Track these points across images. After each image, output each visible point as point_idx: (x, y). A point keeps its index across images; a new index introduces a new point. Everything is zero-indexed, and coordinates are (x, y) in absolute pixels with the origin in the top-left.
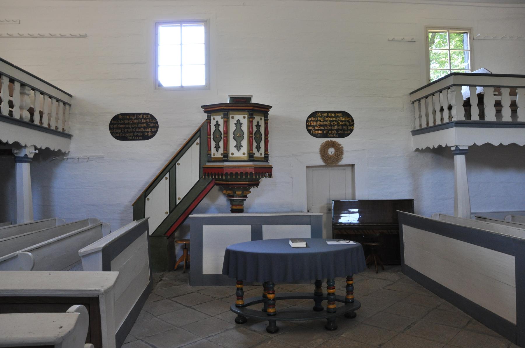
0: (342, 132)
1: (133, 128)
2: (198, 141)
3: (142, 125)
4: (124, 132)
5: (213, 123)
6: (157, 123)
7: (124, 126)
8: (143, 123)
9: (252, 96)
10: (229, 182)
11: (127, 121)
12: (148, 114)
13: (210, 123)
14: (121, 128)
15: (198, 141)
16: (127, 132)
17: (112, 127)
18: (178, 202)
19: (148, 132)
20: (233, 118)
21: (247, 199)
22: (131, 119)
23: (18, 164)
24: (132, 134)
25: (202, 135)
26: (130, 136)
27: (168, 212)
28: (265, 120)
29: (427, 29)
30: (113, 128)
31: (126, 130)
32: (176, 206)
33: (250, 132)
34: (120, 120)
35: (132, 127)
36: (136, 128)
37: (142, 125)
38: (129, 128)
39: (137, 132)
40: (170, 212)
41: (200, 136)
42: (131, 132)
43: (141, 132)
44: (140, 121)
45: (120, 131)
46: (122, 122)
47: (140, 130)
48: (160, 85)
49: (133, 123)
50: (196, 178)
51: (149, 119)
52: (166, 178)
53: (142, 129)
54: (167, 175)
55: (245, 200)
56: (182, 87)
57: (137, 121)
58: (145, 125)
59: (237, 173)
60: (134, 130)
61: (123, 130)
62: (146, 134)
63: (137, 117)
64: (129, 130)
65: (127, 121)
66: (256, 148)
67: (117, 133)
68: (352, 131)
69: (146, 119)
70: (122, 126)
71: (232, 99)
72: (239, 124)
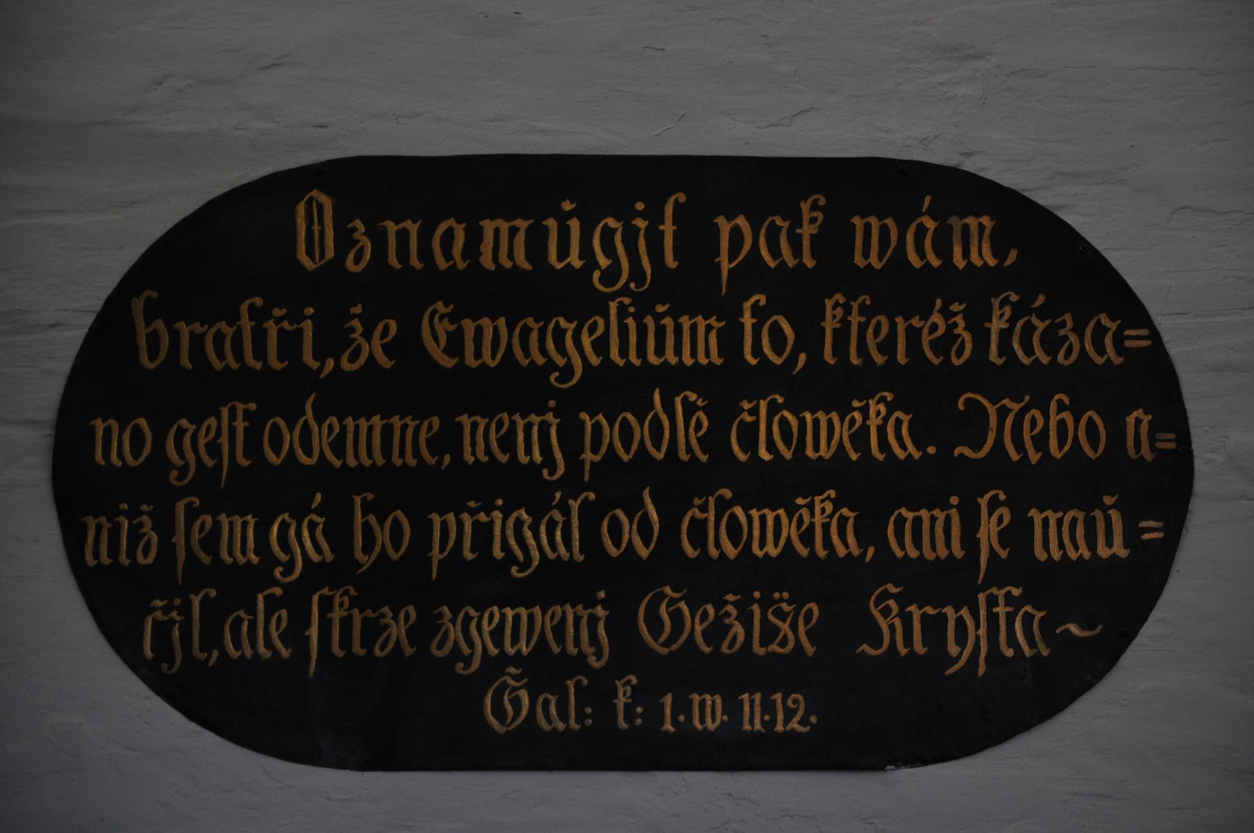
1: (618, 483)
3: (827, 435)
4: (383, 585)
7: (412, 438)
8: (833, 388)
11: (488, 340)
12: (957, 190)
14: (336, 487)
16: (482, 581)
17: (114, 445)
19: (951, 582)
22: (573, 296)
24: (583, 629)
30: (149, 485)
31: (453, 530)
34: (329, 292)
36: (678, 484)
37: (827, 435)
38: (521, 487)
39: (705, 581)
42: (553, 583)
43: (790, 575)
44: (764, 338)
46: (372, 349)
47: (771, 532)
49: (616, 388)
51: (975, 290)
57: (698, 341)
58: (888, 429)
60: (630, 537)
61: (379, 536)
62: (895, 627)
63: (697, 240)
64: (532, 540)
65: (488, 340)
67: (239, 586)
69: (902, 290)
70: (366, 439)
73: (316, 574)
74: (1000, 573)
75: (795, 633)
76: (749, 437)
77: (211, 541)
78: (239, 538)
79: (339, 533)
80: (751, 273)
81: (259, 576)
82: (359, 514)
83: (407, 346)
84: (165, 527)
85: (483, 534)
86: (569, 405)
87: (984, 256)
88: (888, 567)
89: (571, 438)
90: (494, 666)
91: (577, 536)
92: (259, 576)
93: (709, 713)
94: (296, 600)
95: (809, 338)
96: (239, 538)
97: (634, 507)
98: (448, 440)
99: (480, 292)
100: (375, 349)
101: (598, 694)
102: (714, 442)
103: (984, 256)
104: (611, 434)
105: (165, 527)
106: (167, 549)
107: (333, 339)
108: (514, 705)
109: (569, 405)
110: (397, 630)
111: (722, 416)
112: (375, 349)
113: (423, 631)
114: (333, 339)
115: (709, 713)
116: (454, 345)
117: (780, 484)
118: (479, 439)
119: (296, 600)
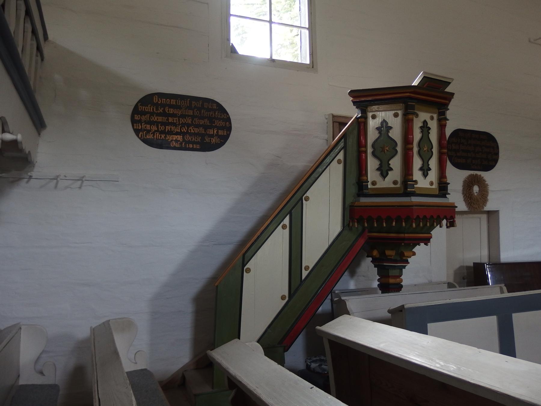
1: (183, 125)
3: (202, 122)
5: (373, 124)
7: (164, 119)
9: (453, 79)
10: (406, 235)
11: (171, 111)
13: (365, 124)
14: (157, 123)
15: (341, 156)
16: (171, 133)
18: (305, 274)
19: (212, 136)
20: (395, 182)
21: (408, 267)
24: (180, 138)
25: (350, 143)
26: (176, 141)
27: (287, 294)
28: (439, 120)
29: (313, 64)
34: (157, 105)
35: (185, 122)
36: (189, 126)
37: (202, 122)
39: (191, 134)
45: (154, 128)
46: (161, 111)
48: (233, 50)
50: (337, 228)
52: (284, 227)
53: (202, 131)
54: (286, 221)
55: (404, 267)
56: (273, 61)
57: (191, 113)
59: (432, 217)
61: (162, 128)
62: (207, 140)
65: (171, 111)
66: (421, 169)
67: (148, 131)
68: (496, 161)
70: (160, 119)
71: (426, 79)
72: (384, 170)
73: (155, 131)
74: (216, 135)
75: (199, 139)
76: (195, 121)
77: (146, 127)
78: (148, 127)
79: (158, 127)
82: (415, 200)
83: (164, 110)
84: (141, 125)
85: (171, 128)
86: (179, 117)
87: (215, 107)
89: (179, 120)
90: (172, 140)
91: (493, 296)
93: (191, 146)
94: (153, 133)
95: (200, 113)
97: (185, 127)
98: (168, 120)
99: (171, 106)
100: (161, 111)
101: (181, 144)
102: (192, 122)
103: (215, 107)
104: (183, 120)
105: (141, 125)
106: (142, 127)
107: (157, 109)
109: (179, 117)
110: (163, 136)
112: (161, 111)
114: (157, 109)
116: (168, 111)
117: (197, 126)
118: (171, 120)
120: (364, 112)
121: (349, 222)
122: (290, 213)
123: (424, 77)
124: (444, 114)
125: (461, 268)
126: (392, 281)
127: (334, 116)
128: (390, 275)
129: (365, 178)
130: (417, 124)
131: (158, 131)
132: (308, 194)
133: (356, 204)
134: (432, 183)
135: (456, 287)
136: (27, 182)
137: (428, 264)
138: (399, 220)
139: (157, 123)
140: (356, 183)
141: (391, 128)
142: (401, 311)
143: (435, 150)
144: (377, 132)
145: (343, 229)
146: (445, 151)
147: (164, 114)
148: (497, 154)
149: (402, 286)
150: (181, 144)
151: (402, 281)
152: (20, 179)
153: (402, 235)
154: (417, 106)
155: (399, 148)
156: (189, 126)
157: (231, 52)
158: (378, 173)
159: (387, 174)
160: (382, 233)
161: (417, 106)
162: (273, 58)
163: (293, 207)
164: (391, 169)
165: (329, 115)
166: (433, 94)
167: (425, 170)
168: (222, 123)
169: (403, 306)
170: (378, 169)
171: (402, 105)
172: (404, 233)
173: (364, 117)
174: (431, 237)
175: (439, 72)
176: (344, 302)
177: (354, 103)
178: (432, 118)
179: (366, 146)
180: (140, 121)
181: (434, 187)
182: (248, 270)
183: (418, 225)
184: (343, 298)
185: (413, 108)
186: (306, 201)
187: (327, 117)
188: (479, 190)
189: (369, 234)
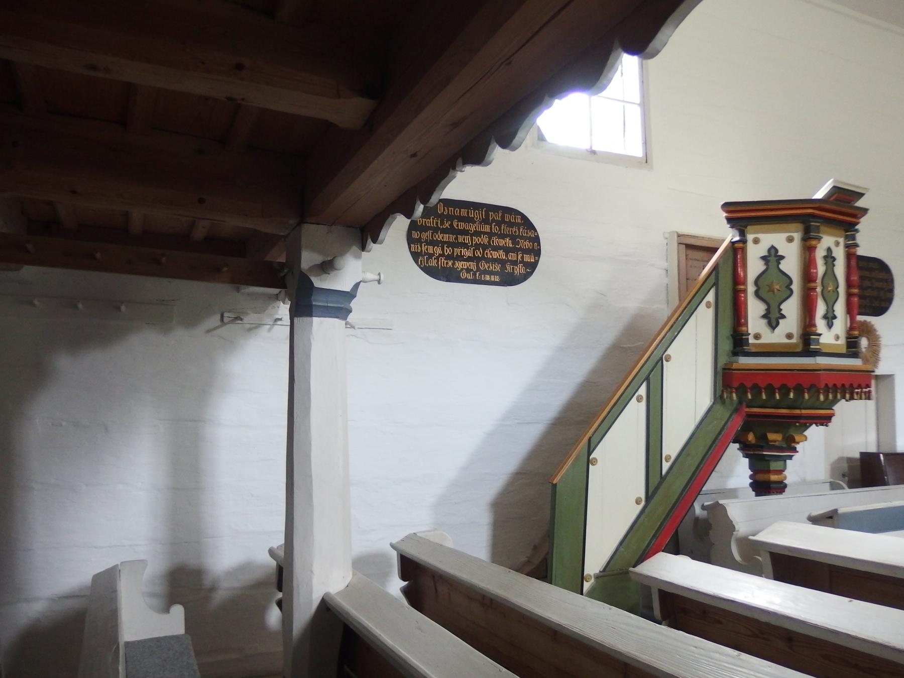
0: (876, 304)
1: (477, 246)
2: (711, 297)
3: (502, 242)
6: (537, 239)
7: (452, 238)
8: (502, 236)
10: (804, 412)
11: (462, 226)
13: (744, 250)
14: (443, 244)
15: (711, 297)
16: (460, 258)
18: (666, 466)
19: (515, 263)
21: (796, 457)
23: (316, 320)
24: (472, 265)
25: (714, 277)
27: (643, 496)
28: (847, 246)
29: (646, 160)
31: (457, 251)
32: (663, 478)
33: (808, 276)
34: (442, 217)
36: (485, 247)
37: (502, 242)
38: (465, 246)
39: (488, 260)
40: (649, 498)
41: (716, 284)
44: (495, 229)
46: (447, 225)
47: (495, 255)
50: (705, 399)
53: (501, 255)
54: (642, 391)
55: (790, 457)
57: (487, 229)
58: (508, 242)
60: (478, 254)
61: (448, 251)
64: (468, 253)
65: (462, 226)
66: (825, 317)
67: (431, 256)
69: (511, 224)
72: (773, 318)
78: (431, 250)
79: (443, 250)
80: (493, 220)
81: (433, 255)
82: (822, 361)
83: (451, 225)
86: (472, 235)
88: (509, 261)
90: (462, 269)
92: (433, 255)
93: (488, 278)
94: (437, 258)
95: (500, 230)
96: (431, 250)
98: (456, 239)
99: (461, 219)
100: (447, 225)
101: (475, 274)
102: (489, 242)
107: (442, 224)
108: (464, 275)
110: (450, 264)
111: (490, 239)
113: (453, 264)
114: (442, 224)
115: (488, 278)
117: (496, 249)
119: (437, 258)
120: (742, 233)
121: (723, 392)
122: (647, 379)
123: (834, 187)
124: (854, 238)
125: (840, 460)
126: (774, 478)
127: (679, 236)
128: (772, 468)
129: (744, 329)
130: (820, 253)
131: (442, 255)
132: (669, 352)
133: (735, 366)
134: (837, 338)
135: (843, 488)
136: (269, 330)
137: (813, 455)
138: (799, 390)
139: (443, 244)
140: (733, 337)
141: (782, 257)
142: (831, 517)
143: (842, 290)
144: (762, 263)
145: (714, 403)
146: (856, 291)
147: (452, 230)
148: (891, 291)
149: (786, 486)
150: (475, 274)
151: (785, 478)
152: (259, 326)
153: (797, 412)
154: (822, 228)
155: (796, 287)
156: (485, 247)
157: (539, 139)
158: (765, 321)
159: (778, 324)
160: (765, 409)
161: (822, 228)
162: (594, 148)
163: (652, 370)
164: (783, 317)
165: (671, 233)
166: (841, 211)
167: (830, 318)
168: (527, 244)
169: (836, 511)
170: (764, 317)
171: (800, 226)
172: (800, 409)
173: (744, 241)
174: (833, 415)
175: (851, 181)
176: (723, 508)
177: (729, 220)
178: (837, 244)
179: (744, 283)
180: (419, 241)
181: (839, 342)
182: (595, 461)
183: (827, 397)
184: (721, 502)
185: (818, 230)
186: (667, 361)
187: (667, 236)
188: (869, 345)
189: (747, 410)
